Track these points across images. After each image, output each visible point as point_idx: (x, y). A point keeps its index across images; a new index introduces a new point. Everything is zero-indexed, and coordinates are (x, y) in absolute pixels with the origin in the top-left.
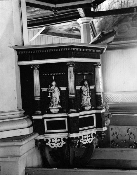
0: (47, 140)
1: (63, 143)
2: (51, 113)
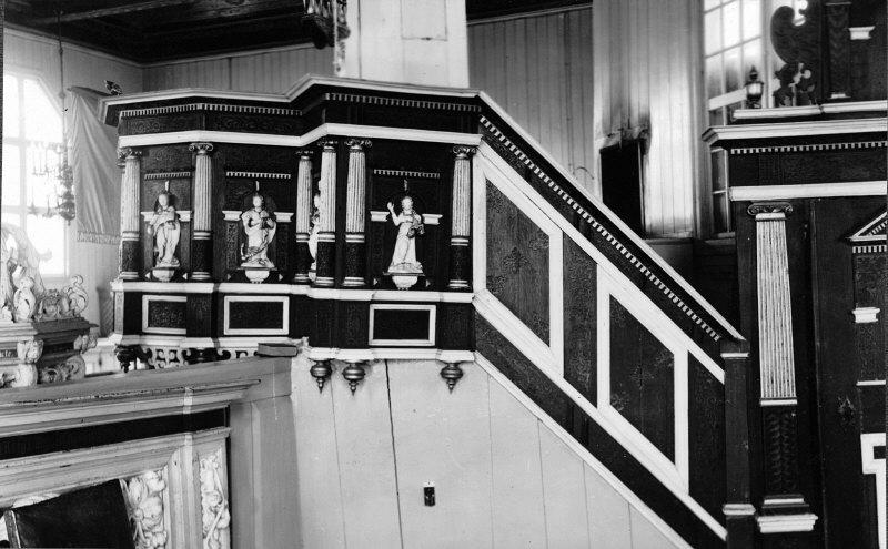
2: (393, 287)
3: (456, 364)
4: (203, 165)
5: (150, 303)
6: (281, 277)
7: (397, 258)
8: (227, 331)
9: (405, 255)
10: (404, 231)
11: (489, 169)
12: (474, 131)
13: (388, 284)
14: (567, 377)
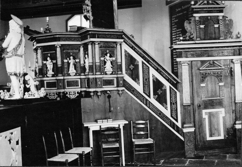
0: (67, 93)
1: (77, 95)
2: (106, 74)
5: (47, 82)
6: (78, 74)
8: (66, 88)
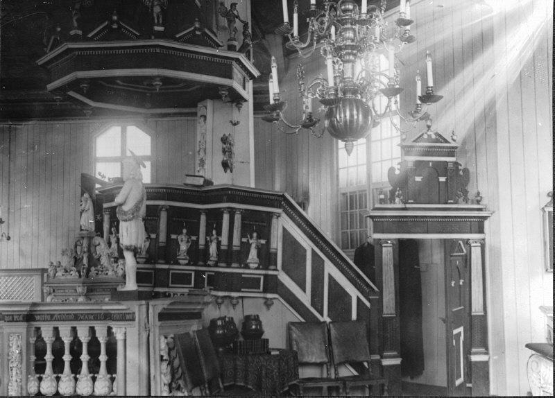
3: (271, 299)
4: (164, 215)
7: (250, 257)
9: (253, 253)
10: (253, 246)
11: (283, 223)
12: (280, 208)
13: (247, 267)
14: (312, 305)
